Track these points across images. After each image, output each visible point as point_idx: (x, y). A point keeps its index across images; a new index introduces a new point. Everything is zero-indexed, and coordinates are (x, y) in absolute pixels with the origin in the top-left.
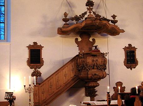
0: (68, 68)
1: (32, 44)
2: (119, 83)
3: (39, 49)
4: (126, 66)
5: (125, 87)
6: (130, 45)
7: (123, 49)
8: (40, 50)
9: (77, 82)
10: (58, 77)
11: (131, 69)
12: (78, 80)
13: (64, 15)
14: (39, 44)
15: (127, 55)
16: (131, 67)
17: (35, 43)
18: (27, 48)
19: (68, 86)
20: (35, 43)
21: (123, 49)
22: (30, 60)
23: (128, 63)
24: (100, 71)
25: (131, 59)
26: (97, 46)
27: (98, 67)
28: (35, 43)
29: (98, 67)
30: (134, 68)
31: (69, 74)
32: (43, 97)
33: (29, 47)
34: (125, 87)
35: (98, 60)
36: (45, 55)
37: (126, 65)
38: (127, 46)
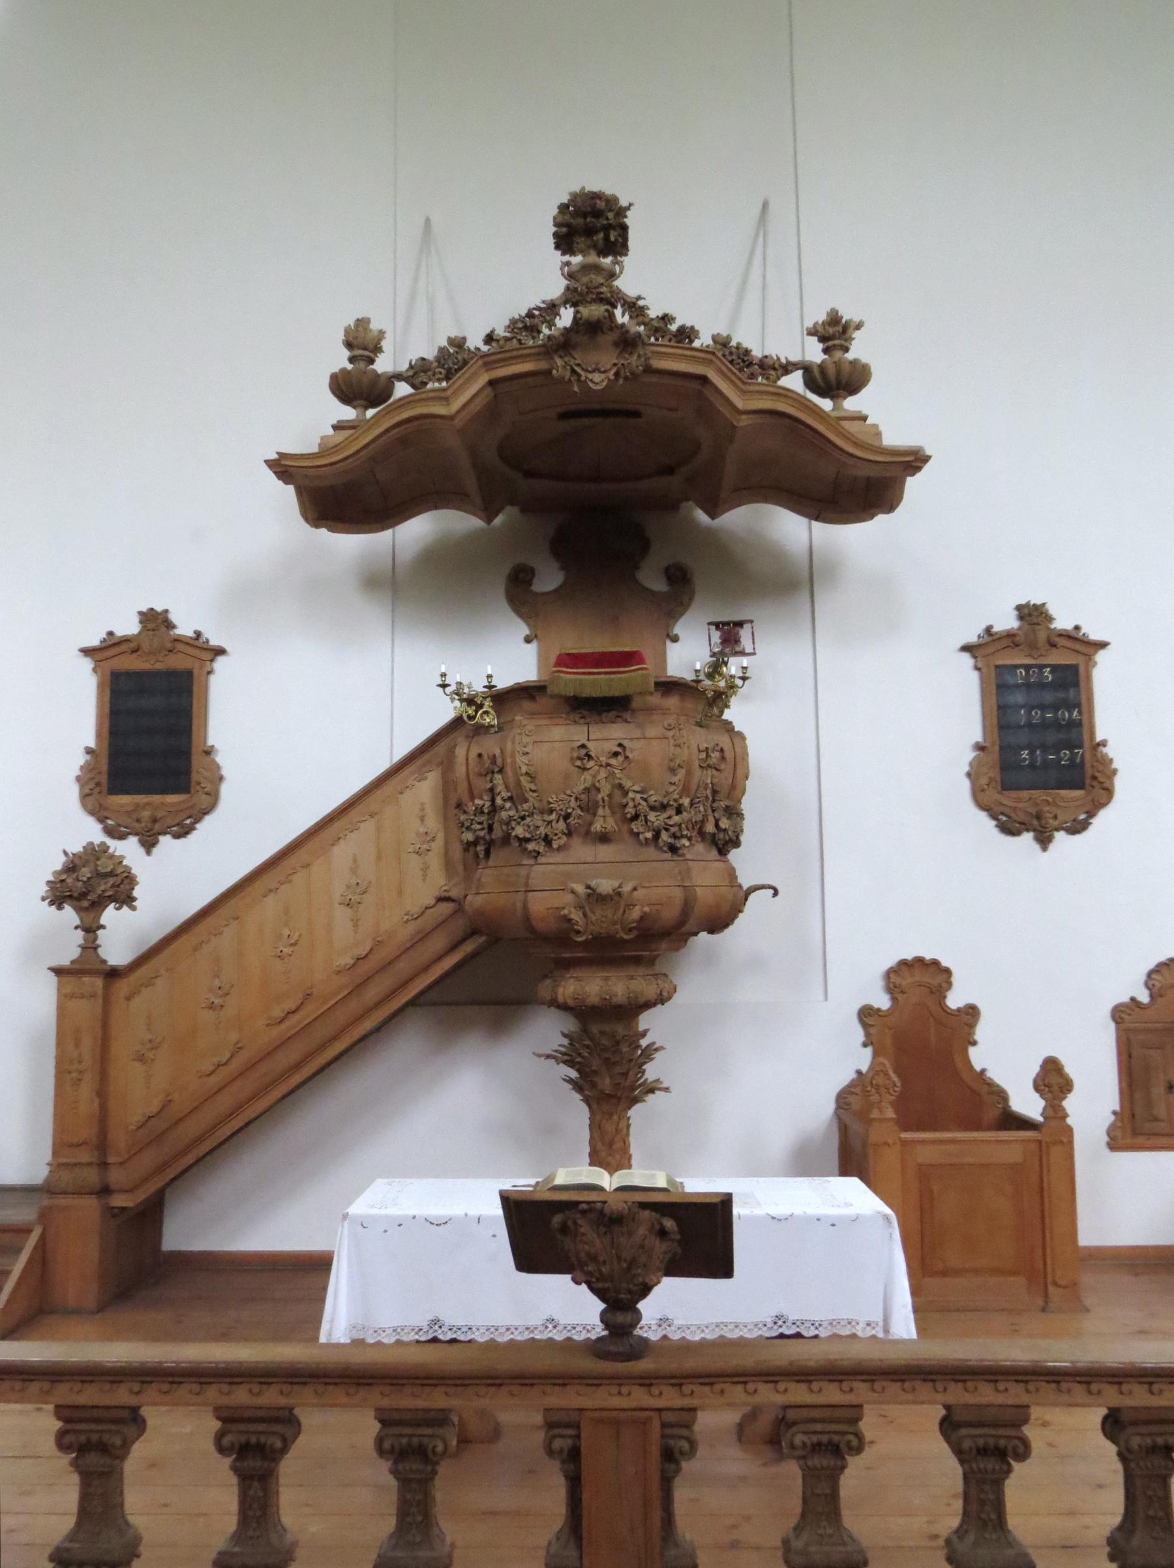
0: (379, 829)
1: (129, 626)
2: (918, 976)
3: (177, 662)
4: (994, 817)
5: (971, 1013)
6: (156, 621)
7: (966, 648)
8: (189, 674)
9: (1143, 1025)
10: (286, 912)
11: (1044, 841)
12: (469, 947)
13: (349, 345)
14: (185, 628)
15: (1002, 708)
16: (1038, 817)
17: (155, 621)
18: (87, 664)
19: (372, 993)
20: (155, 621)
21: (966, 648)
22: (104, 767)
23: (1006, 786)
24: (651, 852)
25: (1039, 747)
26: (740, 624)
27: (636, 817)
28: (156, 621)
29: (636, 817)
30: (1077, 828)
31: (413, 878)
32: (139, 1092)
33: (104, 653)
34: (971, 1013)
35: (635, 749)
36: (233, 719)
37: (993, 795)
38: (129, 626)
